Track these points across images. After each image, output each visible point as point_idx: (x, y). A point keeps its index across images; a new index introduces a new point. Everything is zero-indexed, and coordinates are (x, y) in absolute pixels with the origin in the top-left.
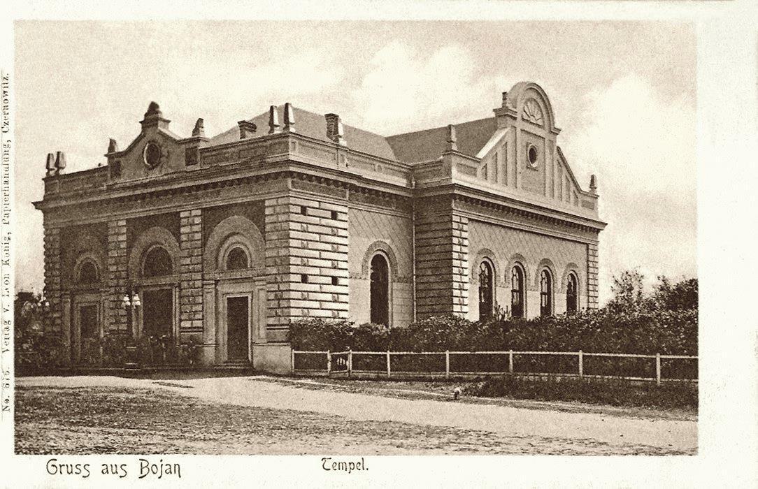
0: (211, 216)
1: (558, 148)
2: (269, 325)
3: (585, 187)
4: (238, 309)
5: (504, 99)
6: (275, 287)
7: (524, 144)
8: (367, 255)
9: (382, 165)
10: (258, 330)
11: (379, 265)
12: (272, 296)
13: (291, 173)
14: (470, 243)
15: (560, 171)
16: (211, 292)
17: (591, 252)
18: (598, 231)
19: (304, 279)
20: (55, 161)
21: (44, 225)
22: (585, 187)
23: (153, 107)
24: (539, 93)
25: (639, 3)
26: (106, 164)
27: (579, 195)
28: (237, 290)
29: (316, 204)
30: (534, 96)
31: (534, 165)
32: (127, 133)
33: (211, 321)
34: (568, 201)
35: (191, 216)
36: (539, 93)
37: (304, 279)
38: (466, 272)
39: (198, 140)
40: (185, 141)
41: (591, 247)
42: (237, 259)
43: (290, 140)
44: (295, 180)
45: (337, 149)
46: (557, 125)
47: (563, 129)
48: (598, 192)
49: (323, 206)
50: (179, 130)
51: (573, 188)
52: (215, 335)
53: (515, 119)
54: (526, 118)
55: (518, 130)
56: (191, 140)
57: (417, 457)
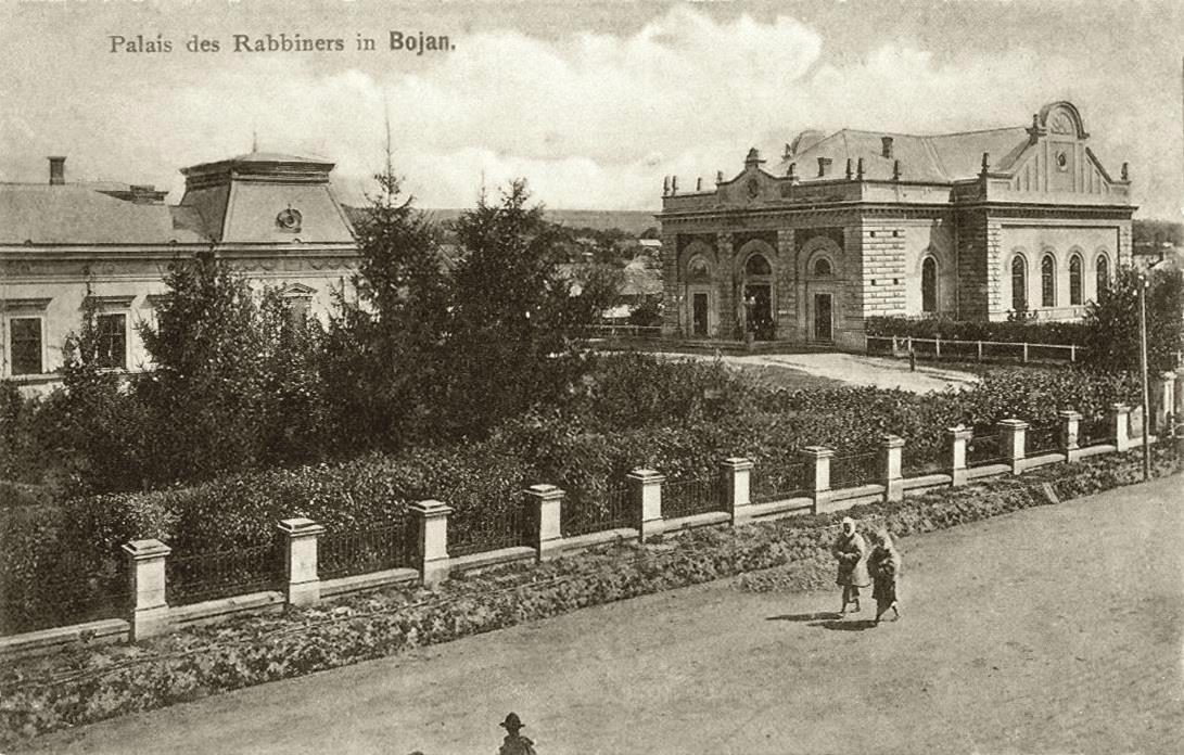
0: (803, 236)
1: (1087, 149)
3: (1116, 176)
4: (823, 303)
5: (1035, 120)
10: (837, 323)
13: (864, 211)
14: (1004, 243)
19: (873, 282)
21: (897, 391)
22: (1116, 176)
23: (753, 152)
25: (1182, 70)
27: (1110, 186)
28: (821, 289)
29: (881, 228)
31: (1063, 168)
32: (734, 168)
33: (802, 309)
35: (786, 235)
37: (873, 282)
38: (999, 267)
39: (792, 179)
42: (822, 267)
48: (1130, 178)
52: (805, 322)
54: (1055, 130)
56: (785, 179)
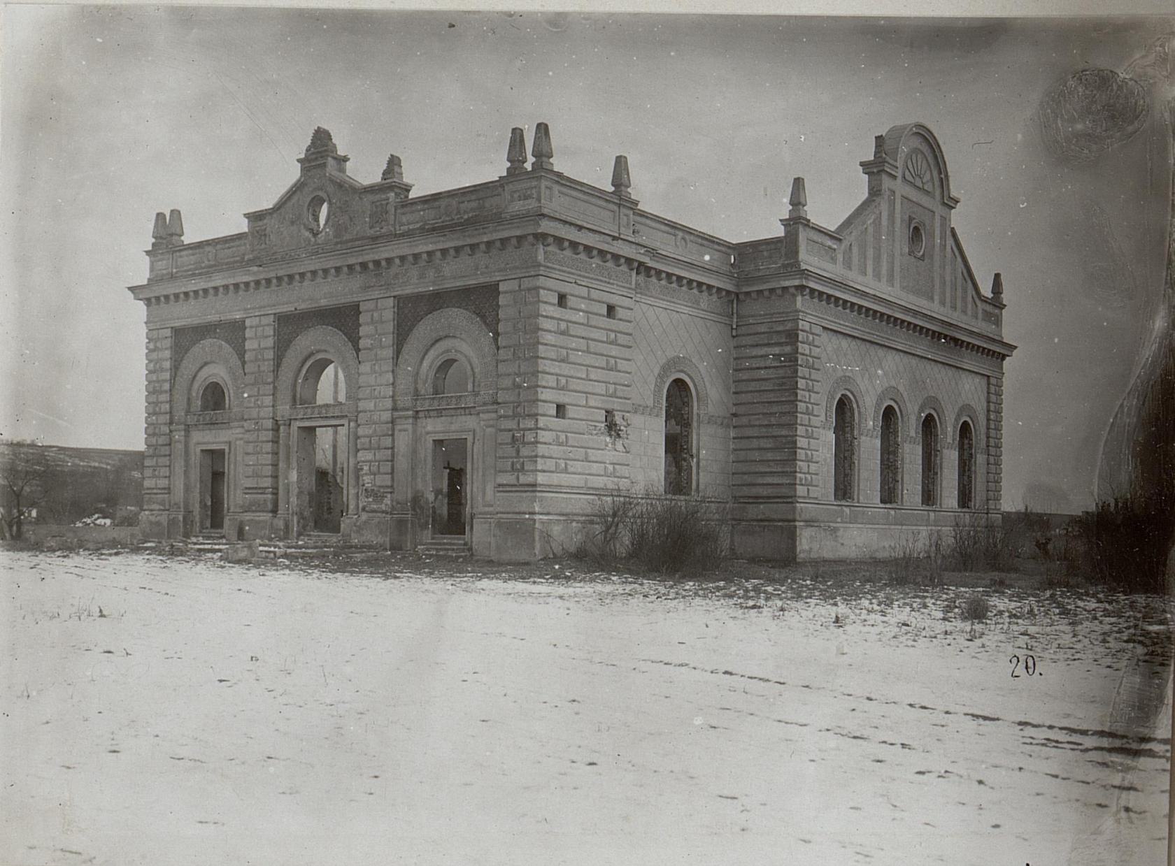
2: (499, 485)
3: (987, 291)
6: (511, 424)
7: (906, 217)
8: (661, 377)
9: (687, 237)
11: (678, 397)
12: (506, 437)
15: (965, 291)
16: (405, 430)
17: (992, 389)
18: (1004, 357)
20: (167, 233)
22: (987, 291)
24: (931, 147)
26: (246, 230)
30: (925, 148)
34: (964, 312)
36: (931, 147)
40: (371, 189)
41: (993, 381)
43: (544, 183)
44: (549, 248)
45: (619, 205)
46: (954, 194)
47: (962, 199)
48: (1006, 297)
49: (595, 294)
50: (365, 170)
51: (971, 291)
53: (895, 177)
55: (898, 195)
57: (107, 2)
